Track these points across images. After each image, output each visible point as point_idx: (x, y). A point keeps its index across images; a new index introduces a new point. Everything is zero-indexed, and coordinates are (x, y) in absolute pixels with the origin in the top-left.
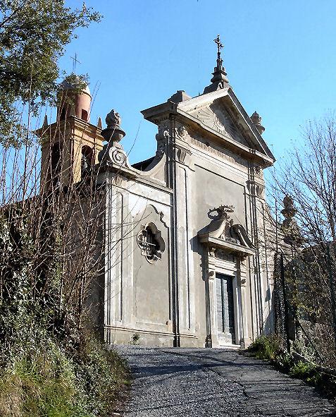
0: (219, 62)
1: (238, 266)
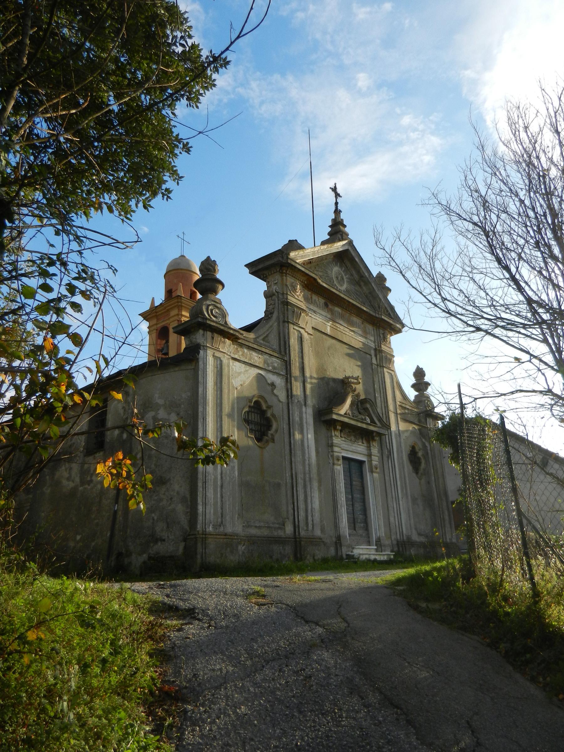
0: (337, 212)
1: (369, 448)
